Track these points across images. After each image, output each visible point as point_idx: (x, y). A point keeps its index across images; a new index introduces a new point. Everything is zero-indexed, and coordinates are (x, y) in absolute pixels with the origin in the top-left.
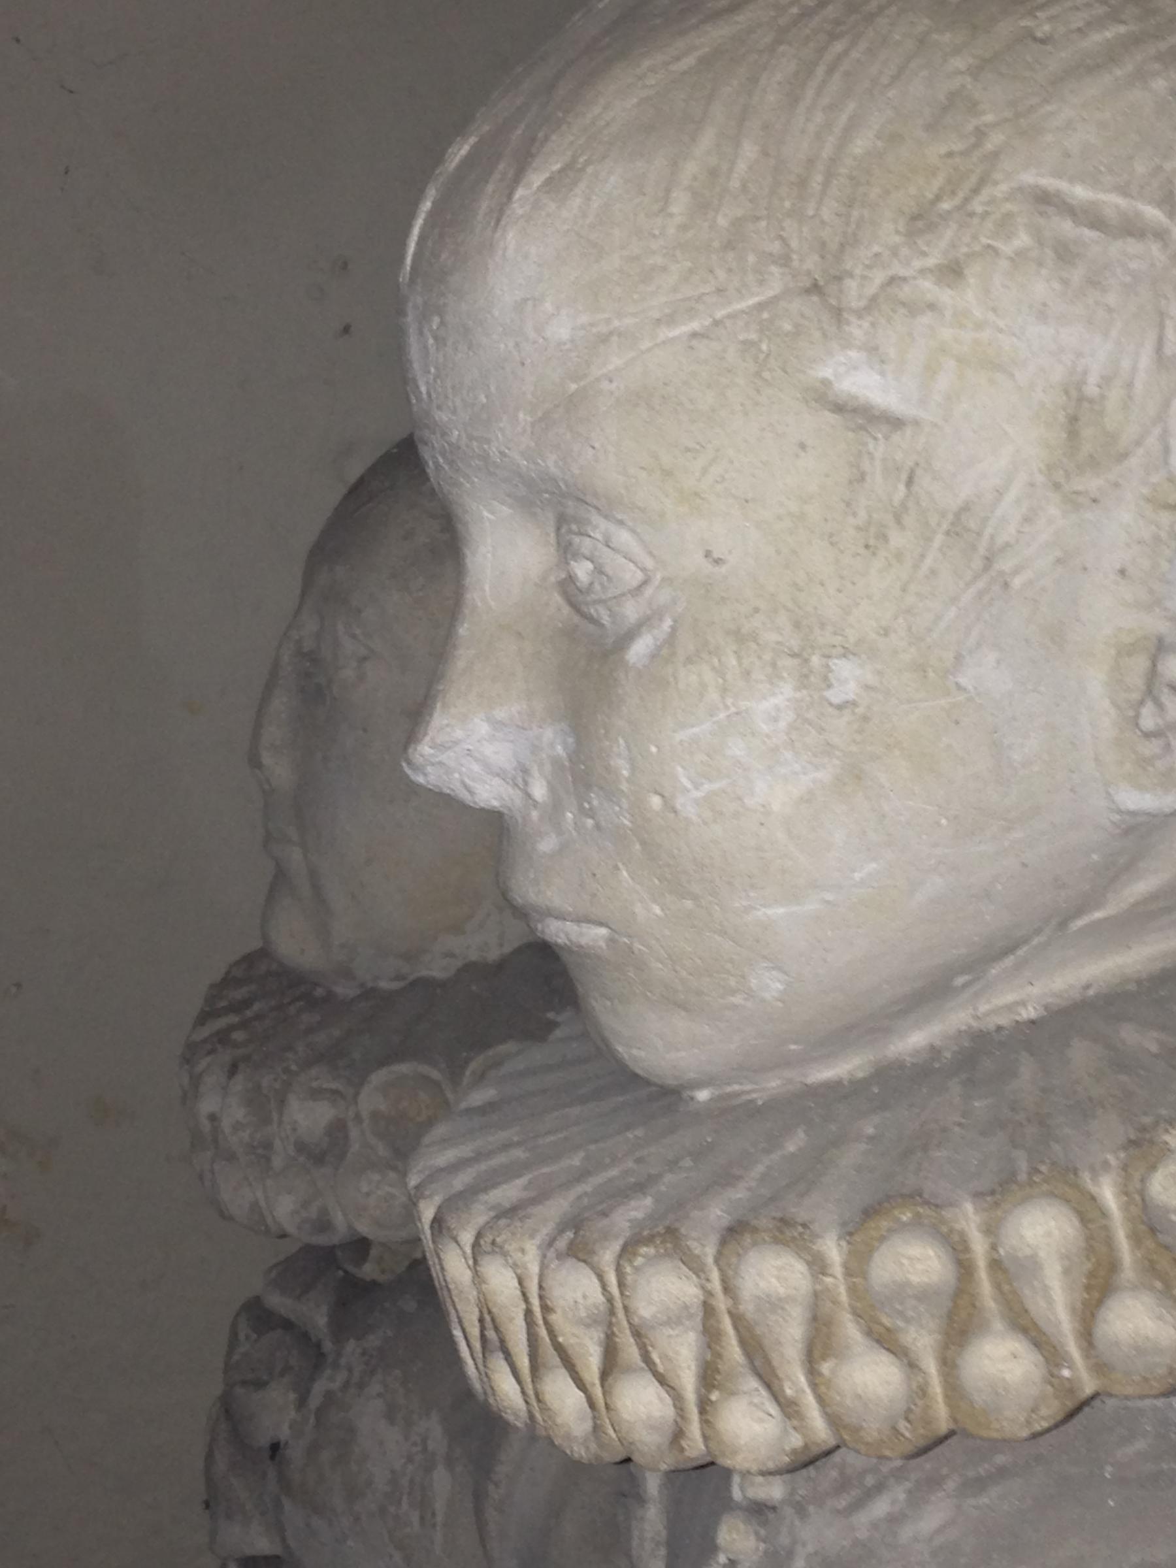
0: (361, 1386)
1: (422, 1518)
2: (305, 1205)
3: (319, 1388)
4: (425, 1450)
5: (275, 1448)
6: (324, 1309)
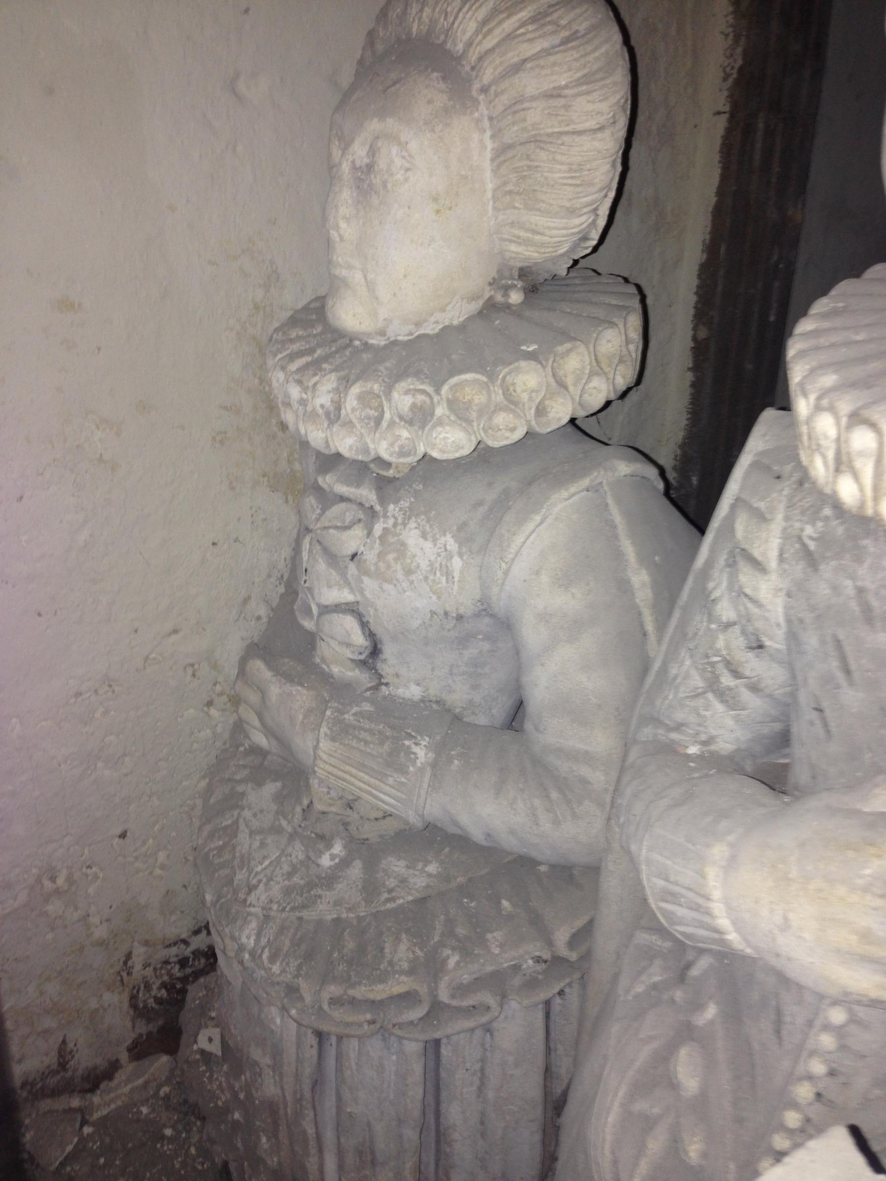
0: (404, 525)
2: (392, 445)
3: (378, 528)
4: (446, 550)
5: (354, 556)
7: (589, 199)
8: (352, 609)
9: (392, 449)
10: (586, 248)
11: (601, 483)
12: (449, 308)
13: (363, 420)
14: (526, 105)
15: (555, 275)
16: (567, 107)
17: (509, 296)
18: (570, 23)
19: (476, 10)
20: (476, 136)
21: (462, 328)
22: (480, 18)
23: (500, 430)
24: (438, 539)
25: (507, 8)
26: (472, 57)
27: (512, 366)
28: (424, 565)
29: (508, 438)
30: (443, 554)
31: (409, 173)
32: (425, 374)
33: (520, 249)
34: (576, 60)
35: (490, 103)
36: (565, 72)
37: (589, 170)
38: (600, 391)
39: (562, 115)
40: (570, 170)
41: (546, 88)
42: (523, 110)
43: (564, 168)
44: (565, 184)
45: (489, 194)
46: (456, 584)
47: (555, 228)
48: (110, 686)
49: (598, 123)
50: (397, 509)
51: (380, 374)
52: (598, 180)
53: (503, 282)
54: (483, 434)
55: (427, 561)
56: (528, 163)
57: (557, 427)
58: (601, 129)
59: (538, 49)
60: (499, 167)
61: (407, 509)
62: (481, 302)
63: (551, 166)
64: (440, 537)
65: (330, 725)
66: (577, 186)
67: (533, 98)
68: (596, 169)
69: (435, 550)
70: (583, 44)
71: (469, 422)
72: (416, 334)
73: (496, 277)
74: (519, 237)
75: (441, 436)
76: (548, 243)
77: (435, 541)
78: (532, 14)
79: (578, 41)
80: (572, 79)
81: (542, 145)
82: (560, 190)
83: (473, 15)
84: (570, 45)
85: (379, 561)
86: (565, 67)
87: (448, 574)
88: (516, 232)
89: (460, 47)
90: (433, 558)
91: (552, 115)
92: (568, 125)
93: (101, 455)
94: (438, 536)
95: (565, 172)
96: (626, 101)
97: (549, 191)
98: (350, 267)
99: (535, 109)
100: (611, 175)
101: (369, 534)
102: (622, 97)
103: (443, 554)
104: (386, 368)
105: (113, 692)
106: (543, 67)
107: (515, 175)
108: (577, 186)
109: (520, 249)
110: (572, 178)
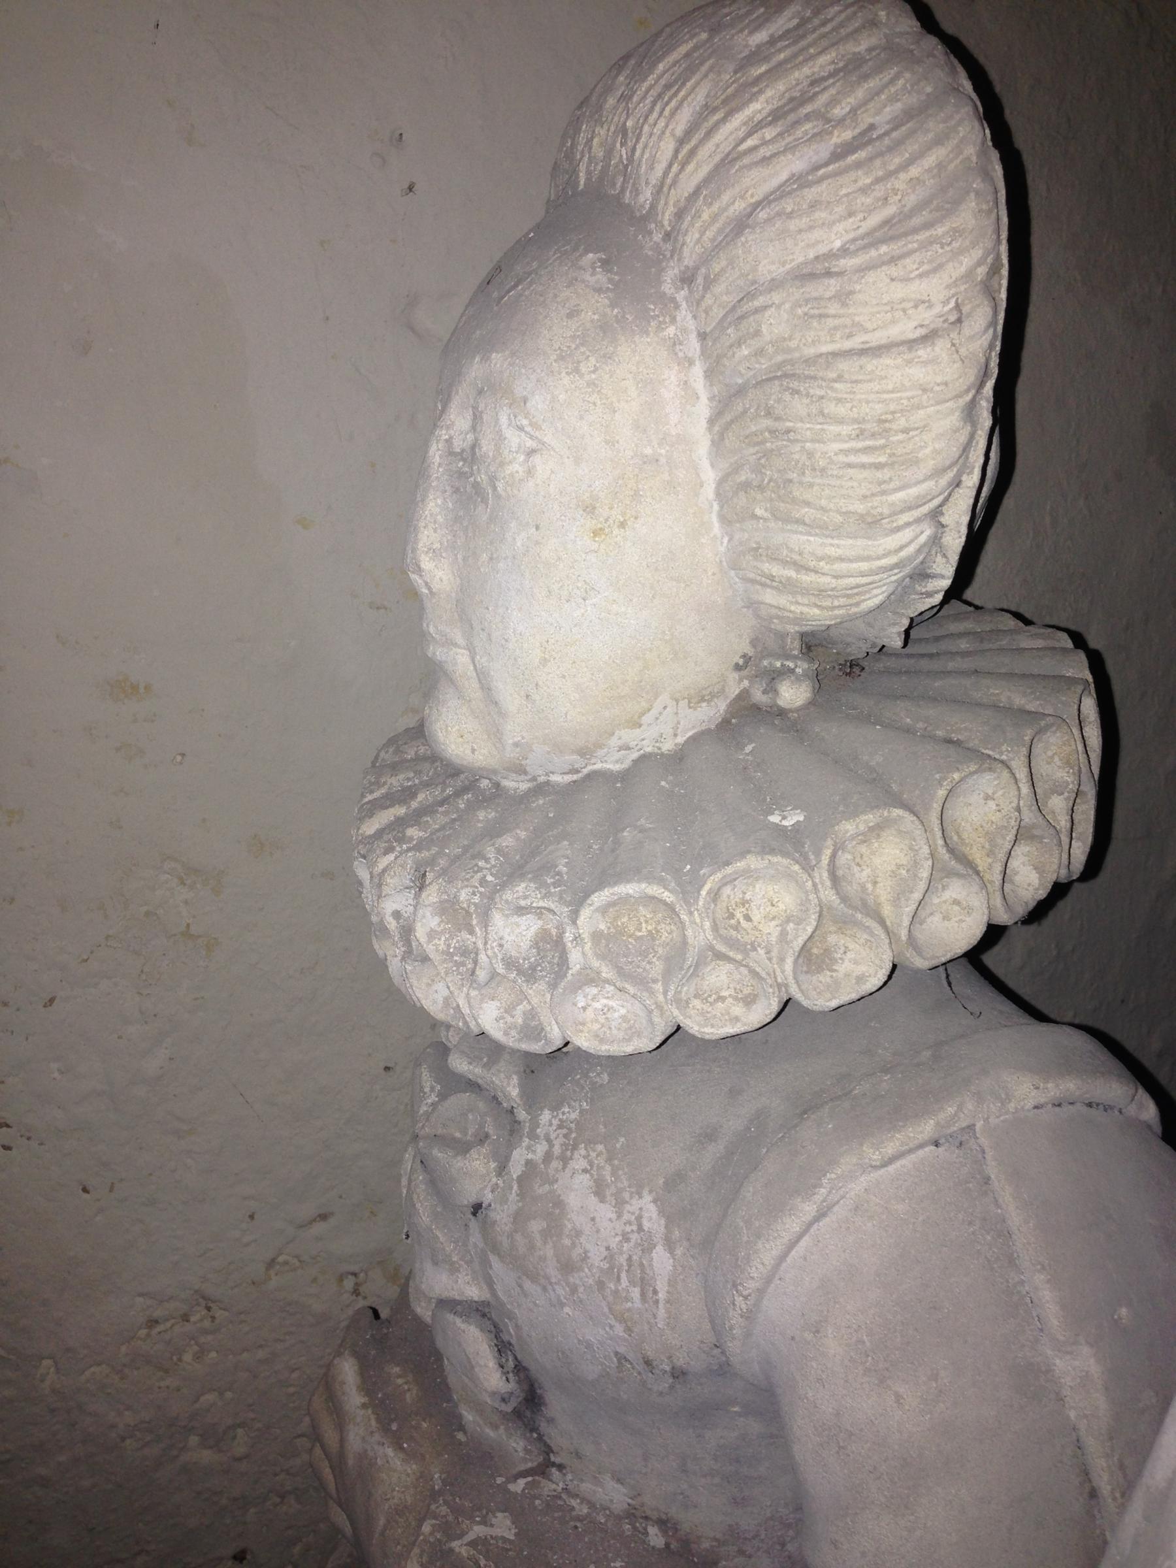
0: (565, 1160)
1: (643, 1294)
2: (509, 1010)
3: (519, 1157)
4: (640, 1229)
5: (477, 1208)
6: (515, 1080)
7: (913, 491)
8: (481, 1312)
9: (509, 1019)
10: (929, 595)
11: (971, 1127)
12: (646, 719)
13: (452, 955)
14: (759, 302)
15: (884, 646)
16: (843, 297)
17: (776, 692)
18: (854, 111)
19: (673, 113)
20: (672, 376)
21: (677, 759)
22: (680, 130)
23: (722, 999)
24: (627, 1202)
25: (725, 102)
26: (663, 213)
27: (729, 870)
28: (597, 1256)
29: (737, 1019)
30: (635, 1237)
31: (537, 459)
32: (559, 873)
33: (782, 601)
34: (864, 190)
35: (698, 304)
36: (842, 219)
37: (905, 431)
38: (969, 910)
39: (834, 316)
40: (860, 435)
41: (801, 259)
42: (756, 311)
43: (846, 430)
44: (850, 466)
45: (709, 491)
46: (661, 1305)
47: (841, 559)
48: (209, 1309)
49: (922, 326)
50: (555, 1122)
51: (481, 863)
52: (928, 451)
53: (765, 663)
54: (676, 1012)
55: (603, 1249)
56: (768, 423)
57: (854, 996)
58: (929, 337)
59: (784, 176)
60: (722, 436)
61: (573, 1126)
62: (722, 706)
63: (819, 427)
64: (631, 1198)
65: (425, 1559)
66: (878, 466)
67: (775, 285)
68: (924, 428)
69: (619, 1226)
70: (881, 154)
71: (643, 982)
72: (585, 771)
73: (750, 652)
74: (772, 578)
75: (598, 1005)
76: (832, 590)
77: (620, 1204)
78: (776, 104)
79: (870, 148)
80: (861, 231)
81: (795, 384)
82: (838, 477)
83: (667, 126)
84: (852, 159)
85: (516, 1232)
86: (840, 209)
87: (645, 1284)
88: (766, 567)
89: (647, 195)
90: (614, 1242)
91: (812, 317)
92: (850, 336)
93: (188, 925)
94: (626, 1195)
95: (850, 438)
96: (994, 270)
97: (818, 481)
98: (449, 643)
99: (779, 307)
100: (963, 438)
101: (502, 1169)
102: (979, 263)
103: (635, 1237)
104: (499, 851)
105: (213, 1318)
106: (790, 216)
107: (752, 450)
108: (878, 466)
109: (782, 601)
110: (866, 450)
